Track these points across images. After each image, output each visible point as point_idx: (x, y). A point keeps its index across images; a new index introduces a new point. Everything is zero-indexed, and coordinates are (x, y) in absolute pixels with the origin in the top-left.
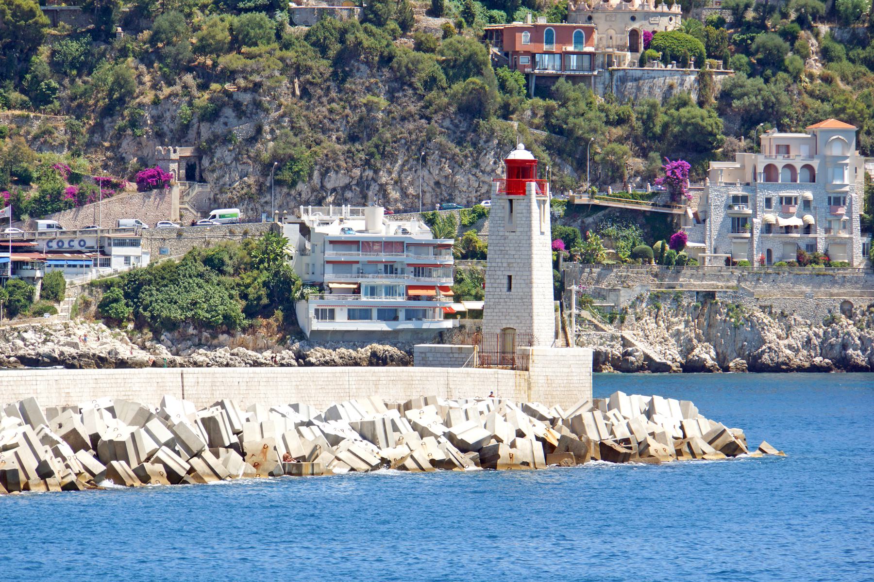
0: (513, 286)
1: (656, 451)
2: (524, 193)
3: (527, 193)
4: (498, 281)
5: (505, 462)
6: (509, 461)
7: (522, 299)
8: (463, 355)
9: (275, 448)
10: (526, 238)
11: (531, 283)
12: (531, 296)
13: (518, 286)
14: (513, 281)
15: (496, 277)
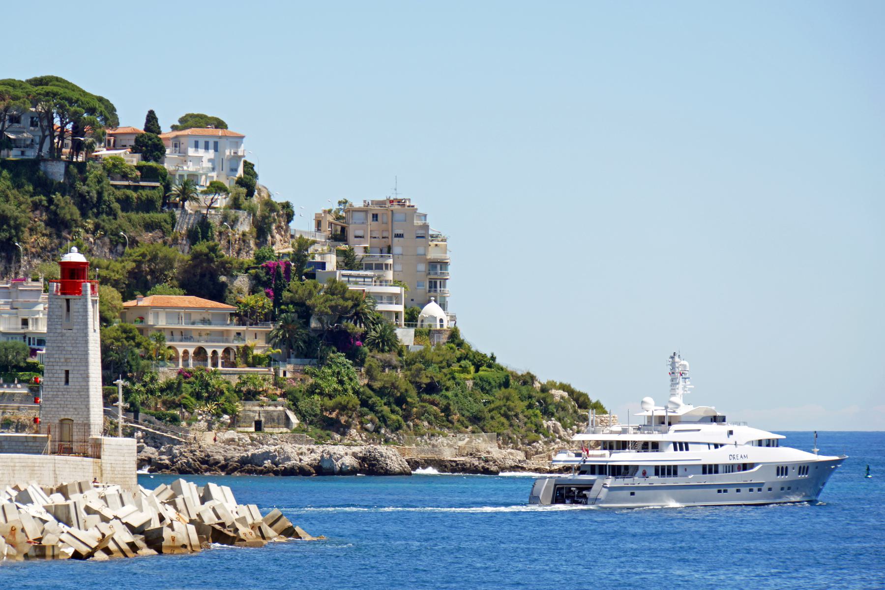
0: (70, 380)
1: (245, 534)
2: (80, 293)
3: (83, 293)
4: (56, 375)
5: (168, 544)
6: (171, 544)
7: (79, 392)
8: (38, 444)
9: (23, 530)
10: (82, 335)
11: (88, 377)
12: (88, 389)
13: (75, 380)
14: (70, 376)
15: (54, 371)
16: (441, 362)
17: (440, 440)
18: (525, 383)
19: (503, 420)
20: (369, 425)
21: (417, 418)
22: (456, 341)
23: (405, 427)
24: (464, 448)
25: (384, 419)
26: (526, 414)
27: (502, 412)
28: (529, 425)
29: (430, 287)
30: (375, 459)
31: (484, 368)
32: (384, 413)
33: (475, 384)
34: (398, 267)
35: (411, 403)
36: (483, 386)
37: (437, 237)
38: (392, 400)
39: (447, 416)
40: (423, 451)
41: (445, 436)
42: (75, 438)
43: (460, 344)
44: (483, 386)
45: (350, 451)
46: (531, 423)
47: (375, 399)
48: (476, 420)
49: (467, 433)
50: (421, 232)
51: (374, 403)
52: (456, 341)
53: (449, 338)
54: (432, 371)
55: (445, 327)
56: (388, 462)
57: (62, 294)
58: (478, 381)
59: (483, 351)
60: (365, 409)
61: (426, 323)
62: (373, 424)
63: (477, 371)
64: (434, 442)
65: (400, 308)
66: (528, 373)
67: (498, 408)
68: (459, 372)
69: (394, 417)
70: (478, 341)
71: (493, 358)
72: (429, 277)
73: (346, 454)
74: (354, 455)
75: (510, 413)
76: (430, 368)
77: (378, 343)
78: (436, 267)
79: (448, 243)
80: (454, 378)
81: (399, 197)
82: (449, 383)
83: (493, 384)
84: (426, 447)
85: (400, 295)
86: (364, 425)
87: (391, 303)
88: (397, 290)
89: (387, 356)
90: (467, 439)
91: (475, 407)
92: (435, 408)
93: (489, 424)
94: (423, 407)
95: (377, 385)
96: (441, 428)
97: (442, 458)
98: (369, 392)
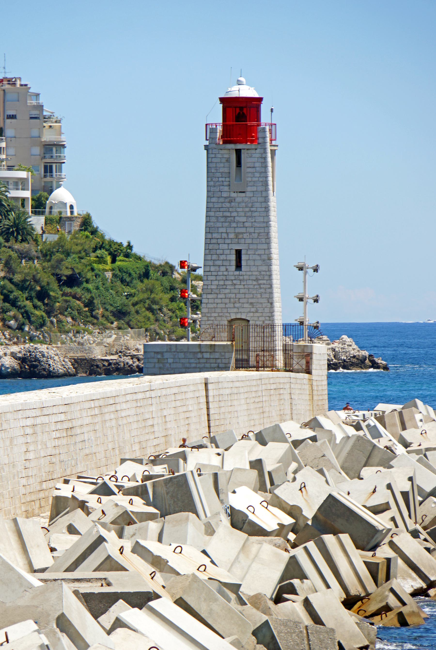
0: (243, 263)
3: (260, 141)
4: (222, 257)
7: (257, 280)
8: (217, 355)
12: (270, 276)
13: (252, 263)
14: (244, 257)
15: (219, 252)
16: (80, 252)
17: (86, 338)
18: (164, 274)
19: (150, 314)
20: (12, 322)
21: (61, 313)
22: (90, 229)
23: (48, 324)
24: (113, 346)
25: (27, 315)
26: (170, 307)
27: (147, 306)
28: (175, 319)
29: (46, 172)
30: (37, 360)
31: (121, 258)
32: (27, 308)
33: (115, 276)
34: (12, 151)
35: (55, 298)
36: (123, 277)
37: (49, 118)
38: (33, 294)
39: (91, 311)
40: (72, 349)
41: (90, 333)
42: (252, 345)
43: (94, 232)
44: (123, 277)
45: (8, 352)
46: (177, 317)
47: (17, 293)
48: (120, 314)
49: (113, 329)
50: (35, 113)
51: (16, 298)
52: (90, 229)
53: (81, 226)
54: (69, 262)
55: (76, 214)
56: (51, 362)
57: (225, 142)
58: (118, 272)
59: (118, 240)
60: (7, 304)
61: (55, 210)
62: (16, 320)
63: (114, 261)
64: (79, 339)
65: (27, 194)
66: (167, 263)
67: (142, 301)
68: (95, 262)
69: (37, 313)
70: (113, 229)
71: (130, 247)
72: (45, 160)
73: (5, 354)
74: (13, 355)
75: (155, 307)
76: (69, 259)
77: (13, 232)
78: (52, 150)
79: (63, 124)
80: (93, 270)
81: (9, 76)
82: (89, 275)
83: (134, 275)
84: (72, 345)
85: (26, 180)
86: (7, 322)
87: (17, 189)
88: (23, 174)
89: (25, 246)
90: (114, 336)
91: (119, 301)
92: (78, 302)
93: (134, 319)
94: (66, 301)
95: (17, 278)
96: (85, 325)
97: (92, 357)
98: (10, 286)
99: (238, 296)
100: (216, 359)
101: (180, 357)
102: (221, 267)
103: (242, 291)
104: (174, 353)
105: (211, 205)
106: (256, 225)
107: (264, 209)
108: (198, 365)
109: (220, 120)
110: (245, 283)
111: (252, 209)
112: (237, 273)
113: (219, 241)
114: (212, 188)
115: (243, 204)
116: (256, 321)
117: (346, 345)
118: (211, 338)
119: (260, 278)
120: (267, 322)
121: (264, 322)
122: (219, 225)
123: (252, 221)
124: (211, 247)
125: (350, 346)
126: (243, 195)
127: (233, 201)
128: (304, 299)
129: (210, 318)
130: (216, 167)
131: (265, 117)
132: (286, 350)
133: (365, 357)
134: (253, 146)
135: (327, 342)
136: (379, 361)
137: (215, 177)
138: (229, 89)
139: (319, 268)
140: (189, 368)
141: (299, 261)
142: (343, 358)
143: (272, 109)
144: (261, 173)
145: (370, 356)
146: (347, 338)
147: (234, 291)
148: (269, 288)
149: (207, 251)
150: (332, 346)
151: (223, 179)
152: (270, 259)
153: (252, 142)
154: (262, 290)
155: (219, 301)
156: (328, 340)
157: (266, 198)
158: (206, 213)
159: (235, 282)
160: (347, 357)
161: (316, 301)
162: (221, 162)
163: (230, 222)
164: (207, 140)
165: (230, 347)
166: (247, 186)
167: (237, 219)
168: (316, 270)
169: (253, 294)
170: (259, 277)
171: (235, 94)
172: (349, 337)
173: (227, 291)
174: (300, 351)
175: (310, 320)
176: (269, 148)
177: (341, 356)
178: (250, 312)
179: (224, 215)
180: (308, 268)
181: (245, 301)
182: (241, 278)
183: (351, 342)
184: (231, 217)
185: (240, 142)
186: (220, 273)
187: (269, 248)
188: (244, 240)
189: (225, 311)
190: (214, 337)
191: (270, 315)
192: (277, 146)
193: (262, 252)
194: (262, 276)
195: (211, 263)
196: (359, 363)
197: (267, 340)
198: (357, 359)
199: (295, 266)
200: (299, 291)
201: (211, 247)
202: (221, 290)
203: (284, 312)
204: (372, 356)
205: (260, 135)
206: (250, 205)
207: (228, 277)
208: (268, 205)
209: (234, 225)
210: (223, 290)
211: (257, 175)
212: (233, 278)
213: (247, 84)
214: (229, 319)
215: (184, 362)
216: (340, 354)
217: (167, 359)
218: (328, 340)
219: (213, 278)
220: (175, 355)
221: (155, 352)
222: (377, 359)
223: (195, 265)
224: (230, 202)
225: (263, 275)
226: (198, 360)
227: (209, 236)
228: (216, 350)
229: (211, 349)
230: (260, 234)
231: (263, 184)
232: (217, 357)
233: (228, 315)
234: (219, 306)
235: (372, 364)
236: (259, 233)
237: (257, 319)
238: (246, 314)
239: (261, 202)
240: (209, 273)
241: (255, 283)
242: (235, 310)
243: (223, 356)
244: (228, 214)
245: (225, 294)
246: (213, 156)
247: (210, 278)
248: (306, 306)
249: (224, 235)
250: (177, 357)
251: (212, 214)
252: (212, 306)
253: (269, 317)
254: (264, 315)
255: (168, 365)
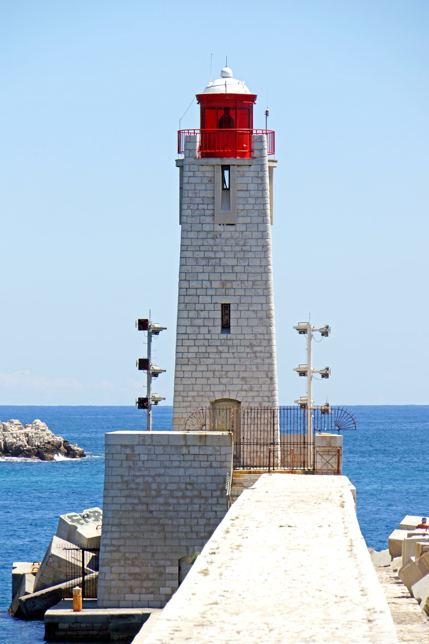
0: (233, 323)
3: (256, 154)
4: (203, 314)
7: (251, 346)
10: (259, 235)
14: (233, 314)
15: (198, 307)
57: (204, 155)
99: (225, 368)
100: (208, 455)
101: (157, 452)
102: (202, 328)
103: (230, 361)
104: (150, 447)
105: (187, 242)
106: (250, 269)
107: (261, 247)
108: (183, 464)
109: (197, 125)
110: (235, 350)
111: (244, 248)
112: (224, 336)
113: (199, 292)
114: (189, 219)
115: (233, 242)
116: (249, 402)
117: (40, 430)
118: (200, 426)
119: (256, 344)
120: (265, 404)
121: (260, 404)
122: (199, 269)
123: (245, 264)
124: (187, 300)
125: (44, 430)
126: (232, 228)
127: (218, 236)
128: (308, 373)
129: (186, 399)
130: (195, 190)
131: (258, 123)
132: (304, 443)
133: (59, 443)
134: (246, 161)
135: (19, 426)
136: (76, 448)
137: (194, 204)
138: (211, 84)
139: (330, 330)
140: (169, 468)
141: (302, 320)
142: (36, 444)
143: (267, 112)
144: (257, 198)
145: (64, 442)
146: (41, 422)
147: (218, 361)
148: (268, 358)
149: (182, 306)
150: (24, 430)
151: (205, 207)
152: (269, 317)
153: (243, 155)
154: (259, 361)
155: (199, 375)
156: (20, 424)
157: (264, 233)
158: (181, 253)
159: (220, 348)
160: (41, 443)
161: (325, 376)
162: (202, 183)
163: (214, 266)
164: (179, 152)
165: (228, 439)
166: (238, 217)
167: (224, 261)
168: (325, 333)
169: (246, 365)
170: (254, 342)
171: (220, 90)
172: (42, 421)
173: (210, 361)
174: (324, 445)
175: (317, 402)
176: (267, 165)
177: (34, 441)
178: (242, 390)
179: (205, 256)
180: (313, 331)
181: (235, 374)
182: (230, 343)
183: (44, 426)
184: (216, 258)
185: (228, 156)
186: (200, 337)
187: (268, 302)
188: (233, 290)
189: (207, 388)
190: (205, 425)
191: (269, 394)
192: (276, 161)
193: (259, 307)
194: (258, 341)
195: (187, 322)
196: (54, 450)
197: (266, 428)
198: (52, 445)
199: (294, 327)
200: (301, 362)
201: (187, 300)
202: (201, 360)
203: (287, 392)
204: (67, 442)
205: (255, 146)
206: (242, 243)
207: (211, 342)
208: (267, 242)
209: (219, 269)
210: (205, 359)
211: (252, 201)
212: (218, 343)
213: (235, 77)
214: (213, 400)
215: (163, 459)
216: (34, 439)
217: (139, 455)
218: (20, 424)
219: (191, 343)
220: (151, 449)
221: (122, 446)
222: (73, 446)
223: (157, 326)
224: (214, 238)
225: (260, 339)
226: (182, 457)
227: (185, 285)
228: (208, 443)
229: (200, 441)
230: (256, 283)
231: (260, 215)
232: (209, 453)
233: (211, 394)
234: (199, 381)
235: (67, 450)
236: (254, 281)
237: (251, 400)
238: (236, 393)
239: (257, 239)
240: (186, 337)
241: (248, 350)
242: (222, 388)
243: (218, 451)
244: (212, 255)
245: (207, 365)
246: (191, 174)
247: (186, 343)
248: (310, 382)
249: (206, 284)
250: (152, 452)
251: (189, 254)
252: (189, 382)
253: (269, 397)
254: (261, 394)
255: (140, 464)
